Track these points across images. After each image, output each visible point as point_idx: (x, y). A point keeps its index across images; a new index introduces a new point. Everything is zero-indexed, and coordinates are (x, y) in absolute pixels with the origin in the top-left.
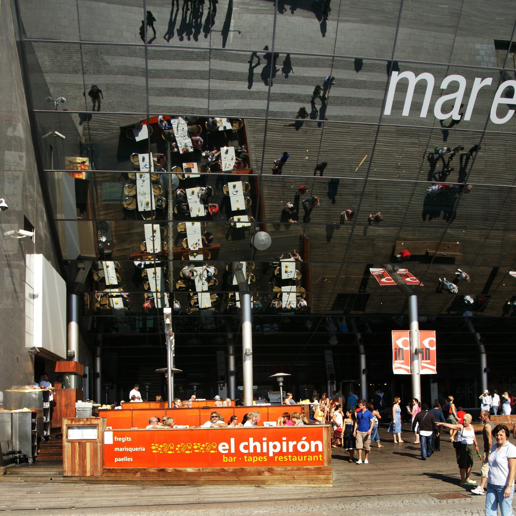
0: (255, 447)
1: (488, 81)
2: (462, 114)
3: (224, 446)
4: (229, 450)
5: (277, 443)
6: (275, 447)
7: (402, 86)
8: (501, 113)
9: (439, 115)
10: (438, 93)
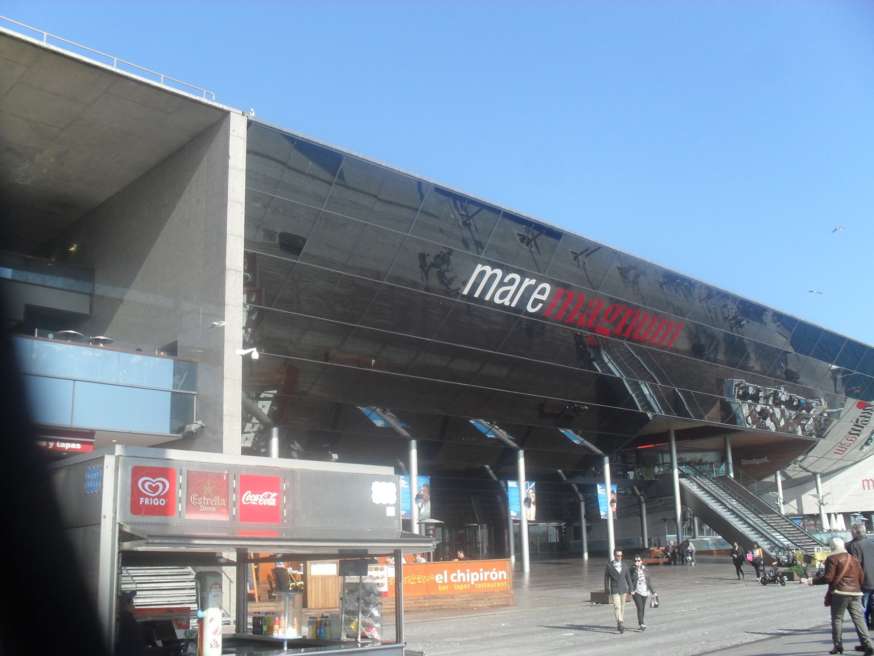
0: (462, 577)
1: (533, 282)
2: (511, 300)
3: (439, 577)
4: (443, 580)
5: (476, 574)
6: (475, 577)
7: (483, 273)
8: (533, 306)
9: (497, 300)
10: (501, 284)
